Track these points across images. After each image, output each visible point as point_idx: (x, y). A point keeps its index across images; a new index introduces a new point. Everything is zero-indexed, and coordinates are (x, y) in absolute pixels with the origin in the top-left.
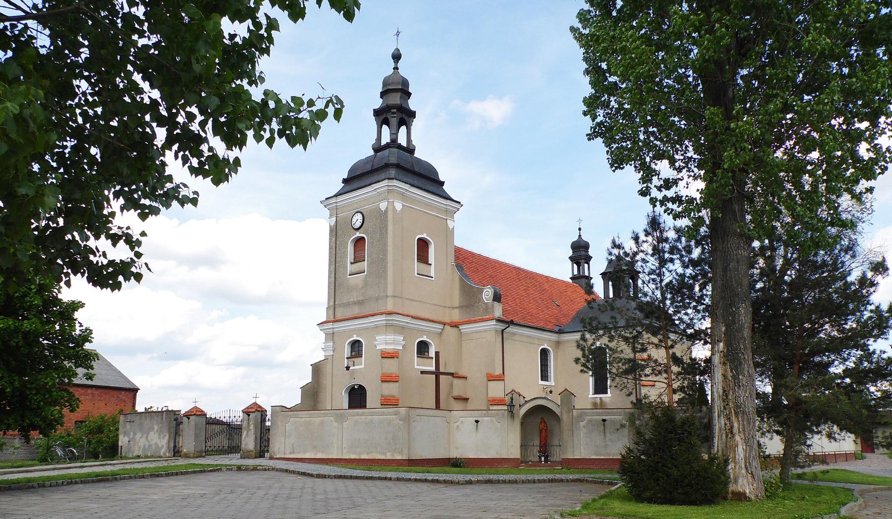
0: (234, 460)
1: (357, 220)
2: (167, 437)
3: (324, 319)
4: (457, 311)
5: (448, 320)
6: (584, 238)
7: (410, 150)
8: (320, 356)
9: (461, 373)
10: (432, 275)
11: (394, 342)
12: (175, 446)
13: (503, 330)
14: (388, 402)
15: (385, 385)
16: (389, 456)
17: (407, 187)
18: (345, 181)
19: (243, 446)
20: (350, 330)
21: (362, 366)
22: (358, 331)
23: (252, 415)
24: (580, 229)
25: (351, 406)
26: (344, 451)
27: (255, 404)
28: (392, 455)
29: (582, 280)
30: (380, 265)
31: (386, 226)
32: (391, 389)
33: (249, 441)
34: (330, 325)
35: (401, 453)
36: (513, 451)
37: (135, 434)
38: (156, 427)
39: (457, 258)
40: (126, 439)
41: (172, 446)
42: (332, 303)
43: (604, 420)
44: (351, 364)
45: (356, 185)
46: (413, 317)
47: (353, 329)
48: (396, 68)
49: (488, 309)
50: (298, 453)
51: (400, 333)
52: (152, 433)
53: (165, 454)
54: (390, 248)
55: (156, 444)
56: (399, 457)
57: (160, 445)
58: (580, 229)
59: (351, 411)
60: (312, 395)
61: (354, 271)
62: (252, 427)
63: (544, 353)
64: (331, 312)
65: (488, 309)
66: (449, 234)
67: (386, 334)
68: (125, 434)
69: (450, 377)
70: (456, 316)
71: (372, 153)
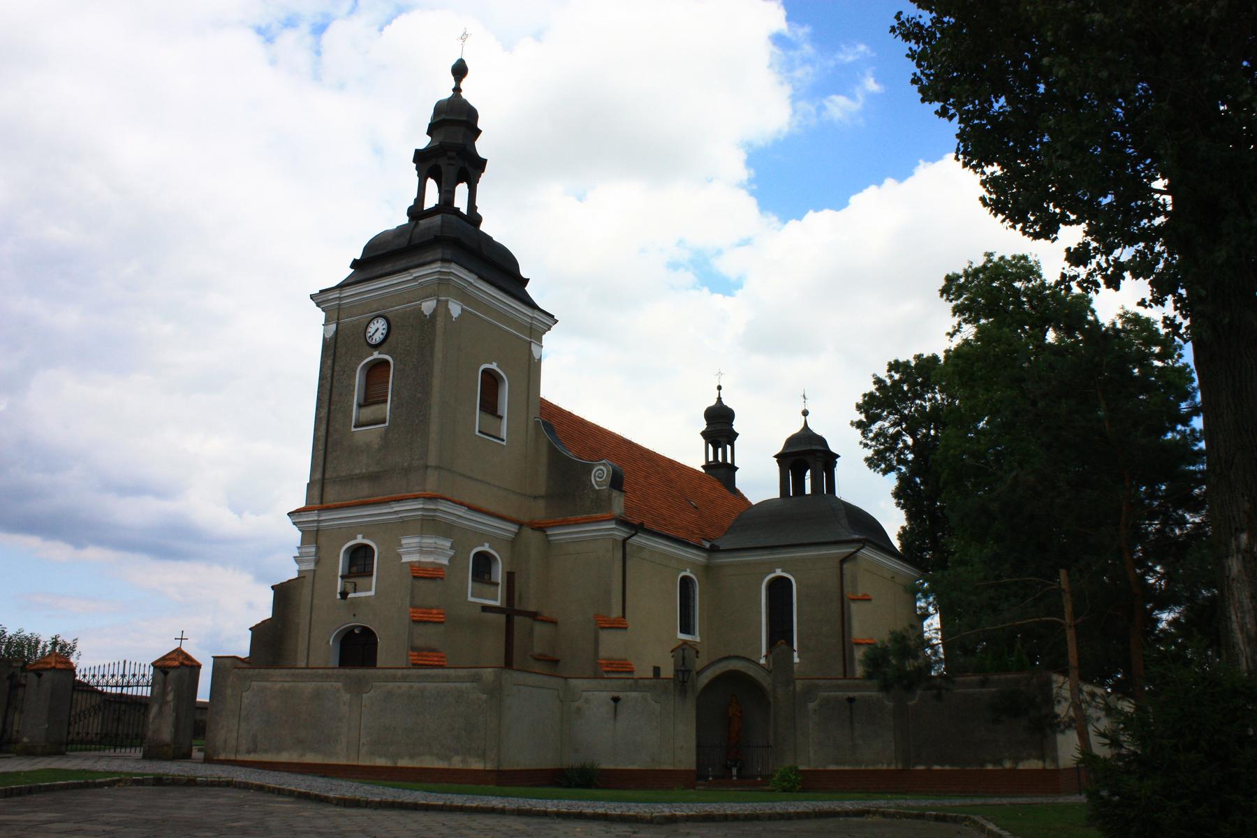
0: (128, 762)
1: (377, 330)
3: (302, 504)
4: (541, 504)
5: (526, 520)
6: (725, 402)
7: (473, 218)
9: (546, 615)
10: (504, 435)
11: (434, 551)
13: (625, 541)
15: (420, 629)
16: (457, 763)
17: (471, 278)
18: (355, 264)
19: (150, 734)
20: (350, 526)
21: (372, 593)
22: (367, 529)
23: (172, 674)
24: (719, 388)
25: (344, 662)
26: (364, 750)
27: (179, 651)
28: (463, 761)
29: (722, 472)
30: (414, 413)
31: (432, 343)
33: (163, 728)
34: (313, 516)
35: (483, 756)
36: (686, 760)
39: (542, 408)
42: (318, 476)
43: (851, 700)
44: (349, 587)
45: (379, 270)
48: (457, 90)
49: (601, 502)
50: (266, 751)
51: (446, 535)
56: (476, 765)
58: (719, 388)
59: (342, 671)
60: (271, 639)
61: (363, 419)
62: (170, 697)
63: (686, 583)
64: (316, 492)
65: (601, 502)
67: (422, 533)
69: (528, 620)
70: (539, 511)
71: (405, 220)
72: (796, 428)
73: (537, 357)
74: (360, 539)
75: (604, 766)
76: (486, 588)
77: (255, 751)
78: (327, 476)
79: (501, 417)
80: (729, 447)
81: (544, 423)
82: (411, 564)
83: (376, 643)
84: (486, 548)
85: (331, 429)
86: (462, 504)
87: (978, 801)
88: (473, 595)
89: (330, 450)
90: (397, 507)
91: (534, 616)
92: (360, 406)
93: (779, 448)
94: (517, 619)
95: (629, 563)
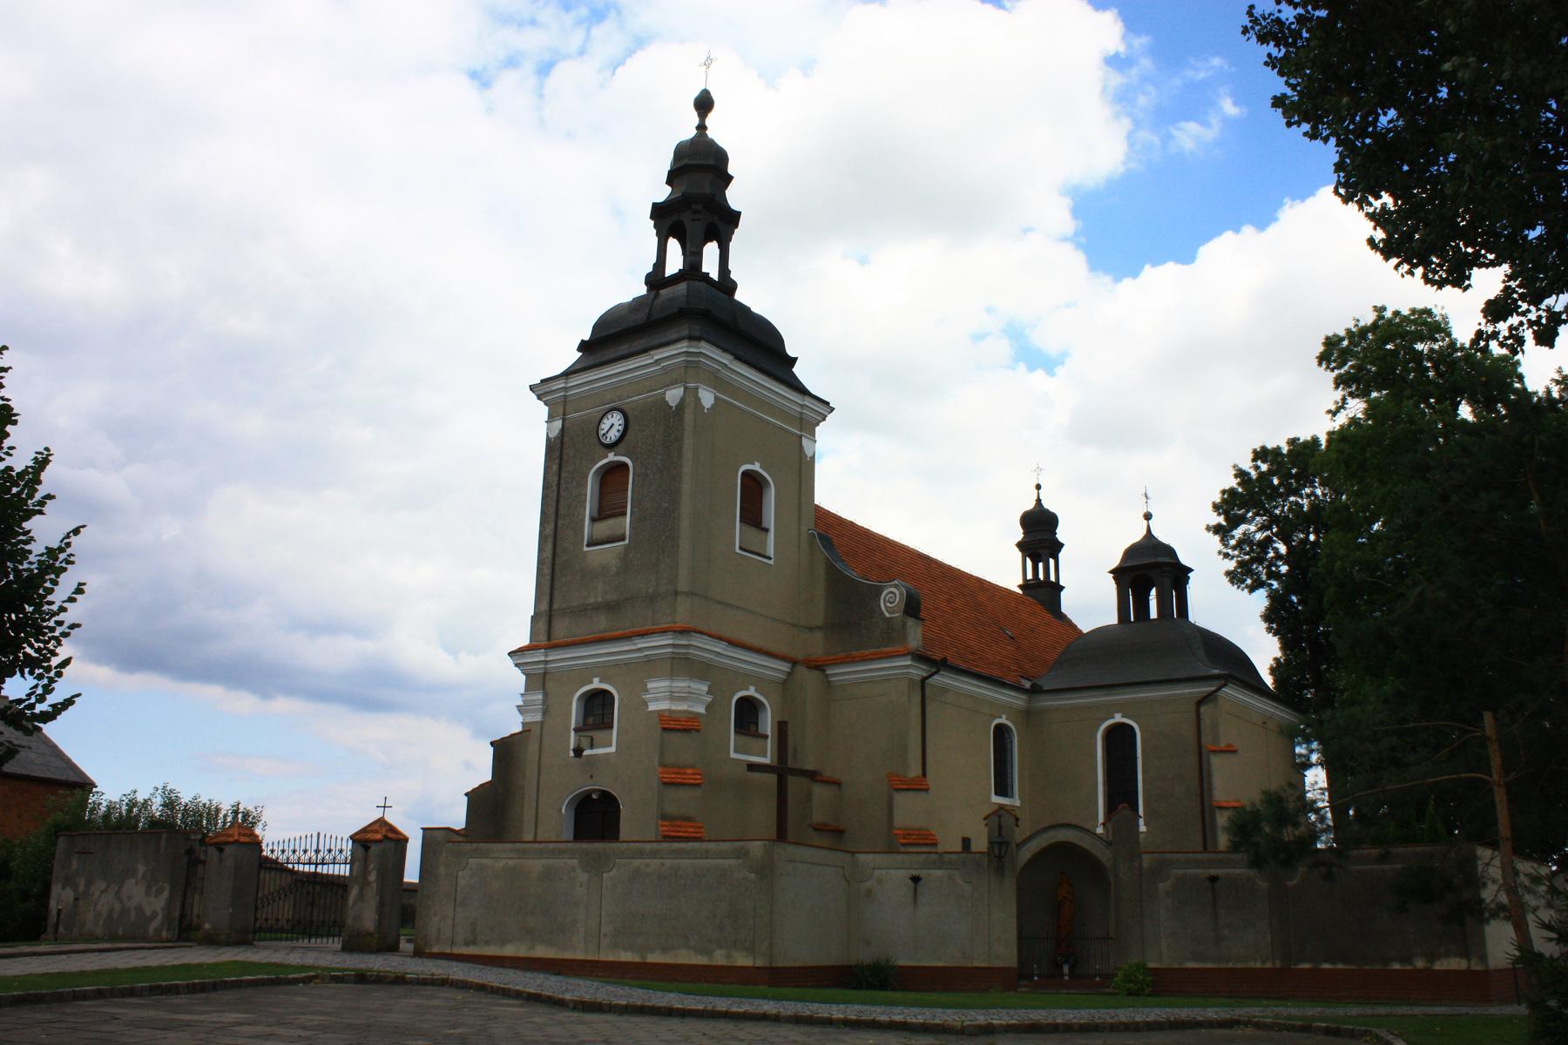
0: (324, 954)
1: (612, 426)
2: (166, 894)
3: (525, 641)
4: (819, 636)
5: (800, 656)
6: (1047, 505)
7: (727, 285)
8: (513, 725)
9: (828, 774)
10: (771, 552)
12: (182, 916)
13: (924, 680)
14: (676, 830)
16: (719, 958)
17: (726, 359)
18: (584, 346)
20: (586, 667)
21: (613, 749)
22: (604, 671)
23: (374, 849)
24: (1038, 487)
26: (605, 942)
27: (381, 822)
28: (728, 957)
29: (1045, 593)
30: (660, 526)
32: (683, 801)
33: (364, 913)
34: (539, 656)
35: (751, 950)
36: (1005, 954)
37: (89, 883)
38: (141, 869)
39: (818, 518)
40: (68, 895)
41: (177, 914)
42: (544, 607)
46: (733, 643)
47: (593, 664)
48: (702, 128)
50: (487, 943)
51: (702, 678)
52: (130, 883)
53: (158, 932)
54: (686, 487)
55: (139, 909)
56: (743, 960)
57: (148, 912)
58: (1038, 487)
59: (577, 845)
62: (372, 877)
64: (543, 626)
66: (802, 471)
68: (68, 882)
70: (816, 645)
71: (642, 290)
72: (1137, 535)
73: (809, 454)
74: (596, 684)
75: (902, 963)
76: (751, 741)
77: (474, 943)
78: (555, 606)
79: (767, 530)
80: (1052, 561)
81: (821, 536)
82: (660, 713)
83: (618, 811)
84: (751, 692)
85: (559, 550)
86: (720, 638)
87: (1382, 1010)
88: (736, 751)
89: (558, 574)
90: (641, 643)
91: (813, 775)
92: (593, 520)
93: (1115, 561)
94: (792, 781)
95: (929, 709)
